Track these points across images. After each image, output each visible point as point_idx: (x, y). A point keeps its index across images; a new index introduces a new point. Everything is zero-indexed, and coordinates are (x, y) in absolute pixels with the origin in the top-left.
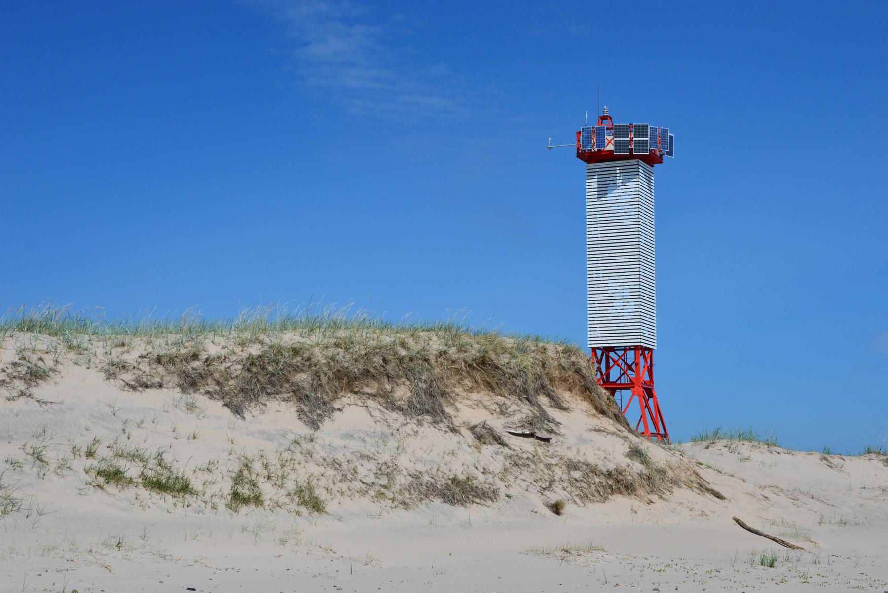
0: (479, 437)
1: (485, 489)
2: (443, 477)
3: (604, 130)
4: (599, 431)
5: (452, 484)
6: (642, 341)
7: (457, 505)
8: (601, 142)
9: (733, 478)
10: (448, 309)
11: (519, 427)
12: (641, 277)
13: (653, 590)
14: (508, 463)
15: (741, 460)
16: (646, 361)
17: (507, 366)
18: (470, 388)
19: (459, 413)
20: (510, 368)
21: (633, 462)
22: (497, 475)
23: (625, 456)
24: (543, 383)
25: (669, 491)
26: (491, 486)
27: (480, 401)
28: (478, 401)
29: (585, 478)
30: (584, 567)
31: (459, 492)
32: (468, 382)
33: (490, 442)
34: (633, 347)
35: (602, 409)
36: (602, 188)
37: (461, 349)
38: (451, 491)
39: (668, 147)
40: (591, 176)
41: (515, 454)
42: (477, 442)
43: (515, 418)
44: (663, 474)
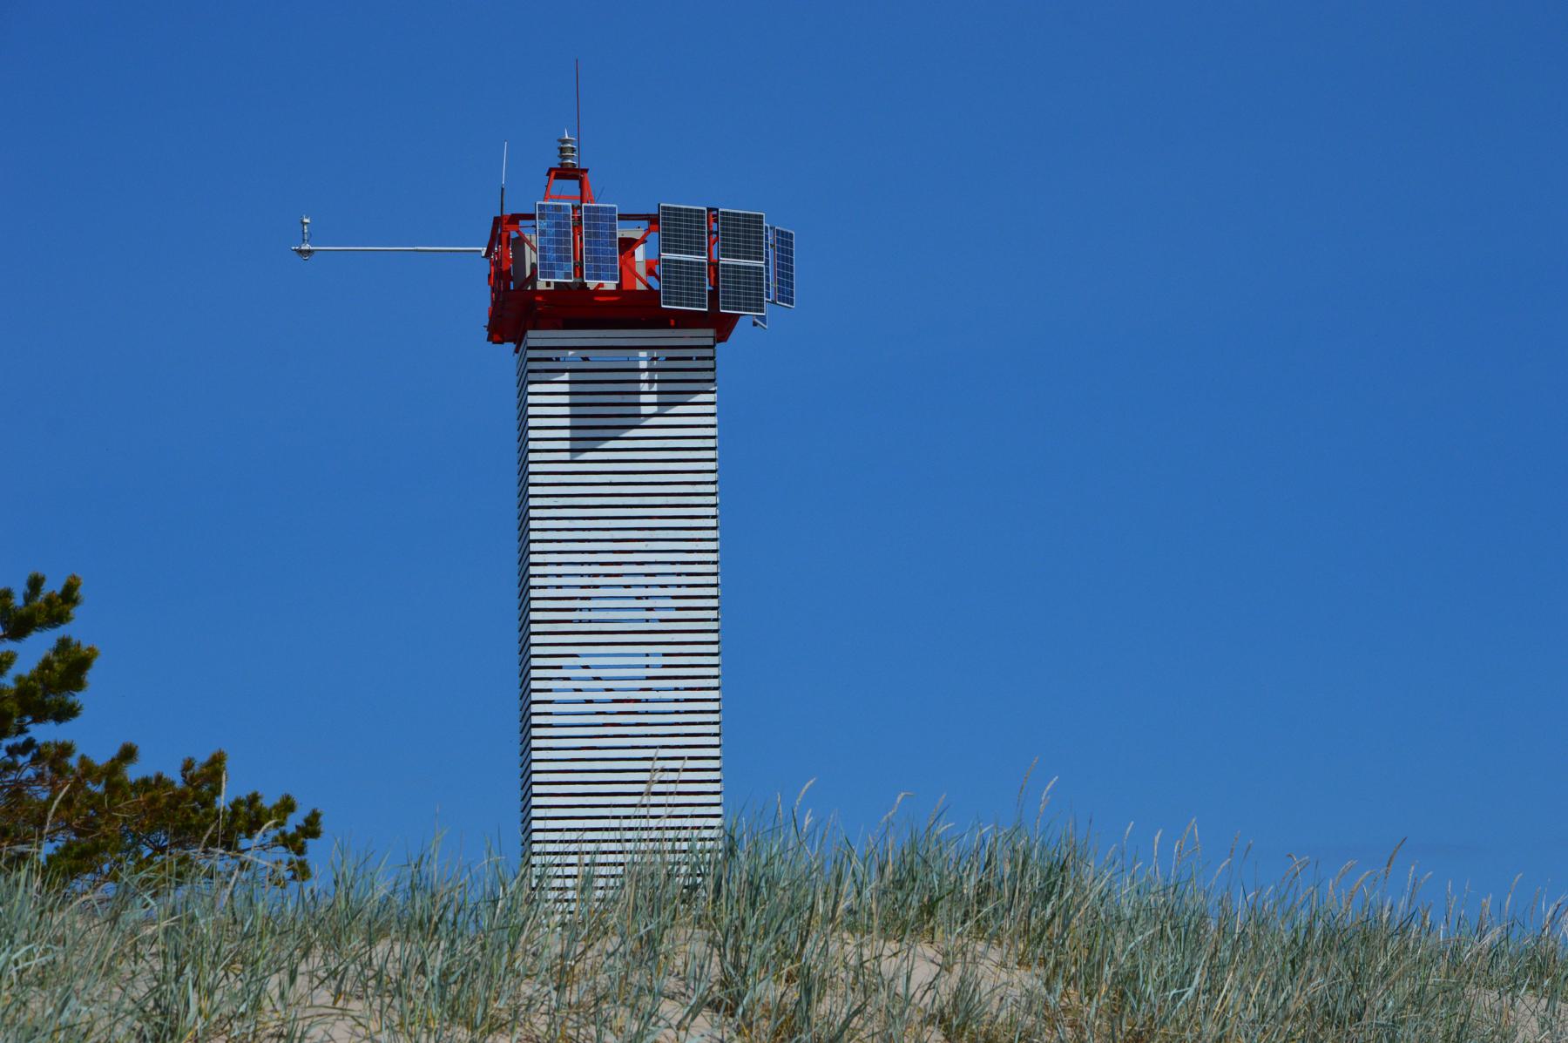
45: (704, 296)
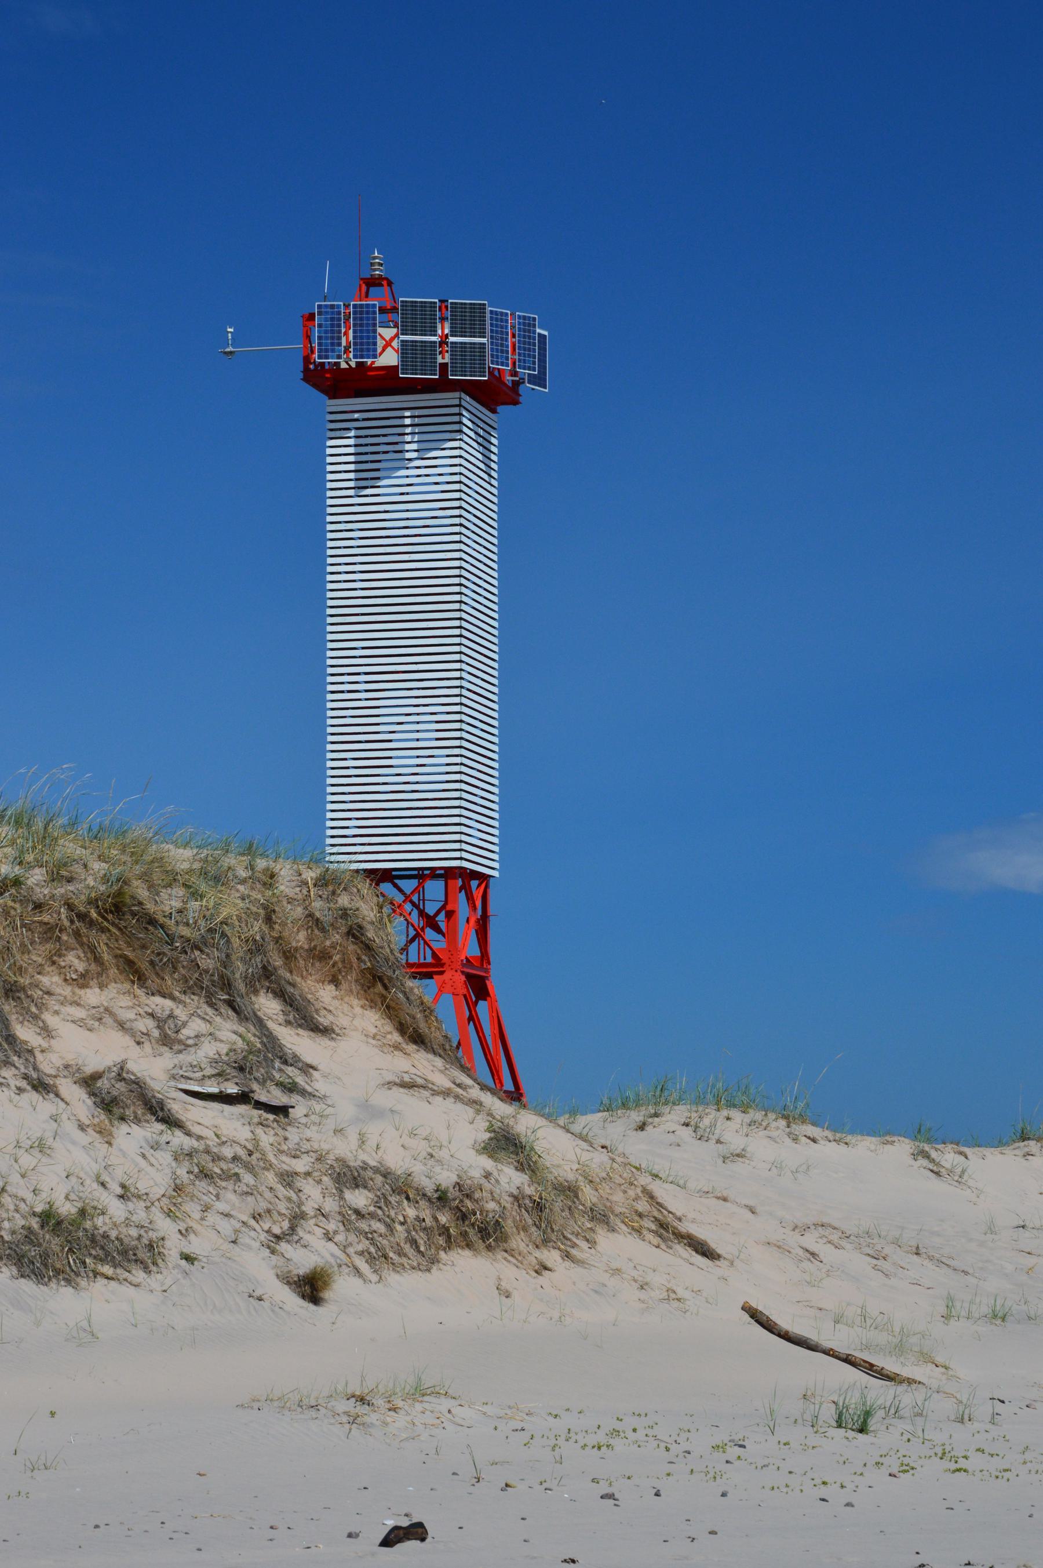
0: (108, 1105)
1: (126, 1240)
2: (17, 1211)
3: (374, 313)
4: (413, 1086)
5: (42, 1227)
6: (465, 855)
7: (53, 1284)
8: (366, 344)
9: (728, 1204)
10: (22, 771)
11: (209, 1077)
12: (465, 692)
13: (602, 1497)
14: (185, 1173)
15: (725, 1159)
16: (474, 908)
17: (178, 918)
18: (83, 976)
19: (53, 1042)
20: (187, 924)
21: (500, 1166)
22: (156, 1204)
23: (477, 1151)
24: (268, 962)
25: (588, 1240)
26: (142, 1232)
27: (107, 1009)
28: (102, 1009)
29: (380, 1208)
30: (407, 1439)
31: (57, 1249)
32: (75, 961)
33: (136, 1117)
34: (442, 872)
35: (415, 1030)
36: (367, 462)
37: (58, 874)
38: (40, 1245)
39: (534, 363)
40: (340, 429)
41: (201, 1148)
42: (103, 1117)
43: (201, 1053)
44: (572, 1194)
45: (436, 366)
